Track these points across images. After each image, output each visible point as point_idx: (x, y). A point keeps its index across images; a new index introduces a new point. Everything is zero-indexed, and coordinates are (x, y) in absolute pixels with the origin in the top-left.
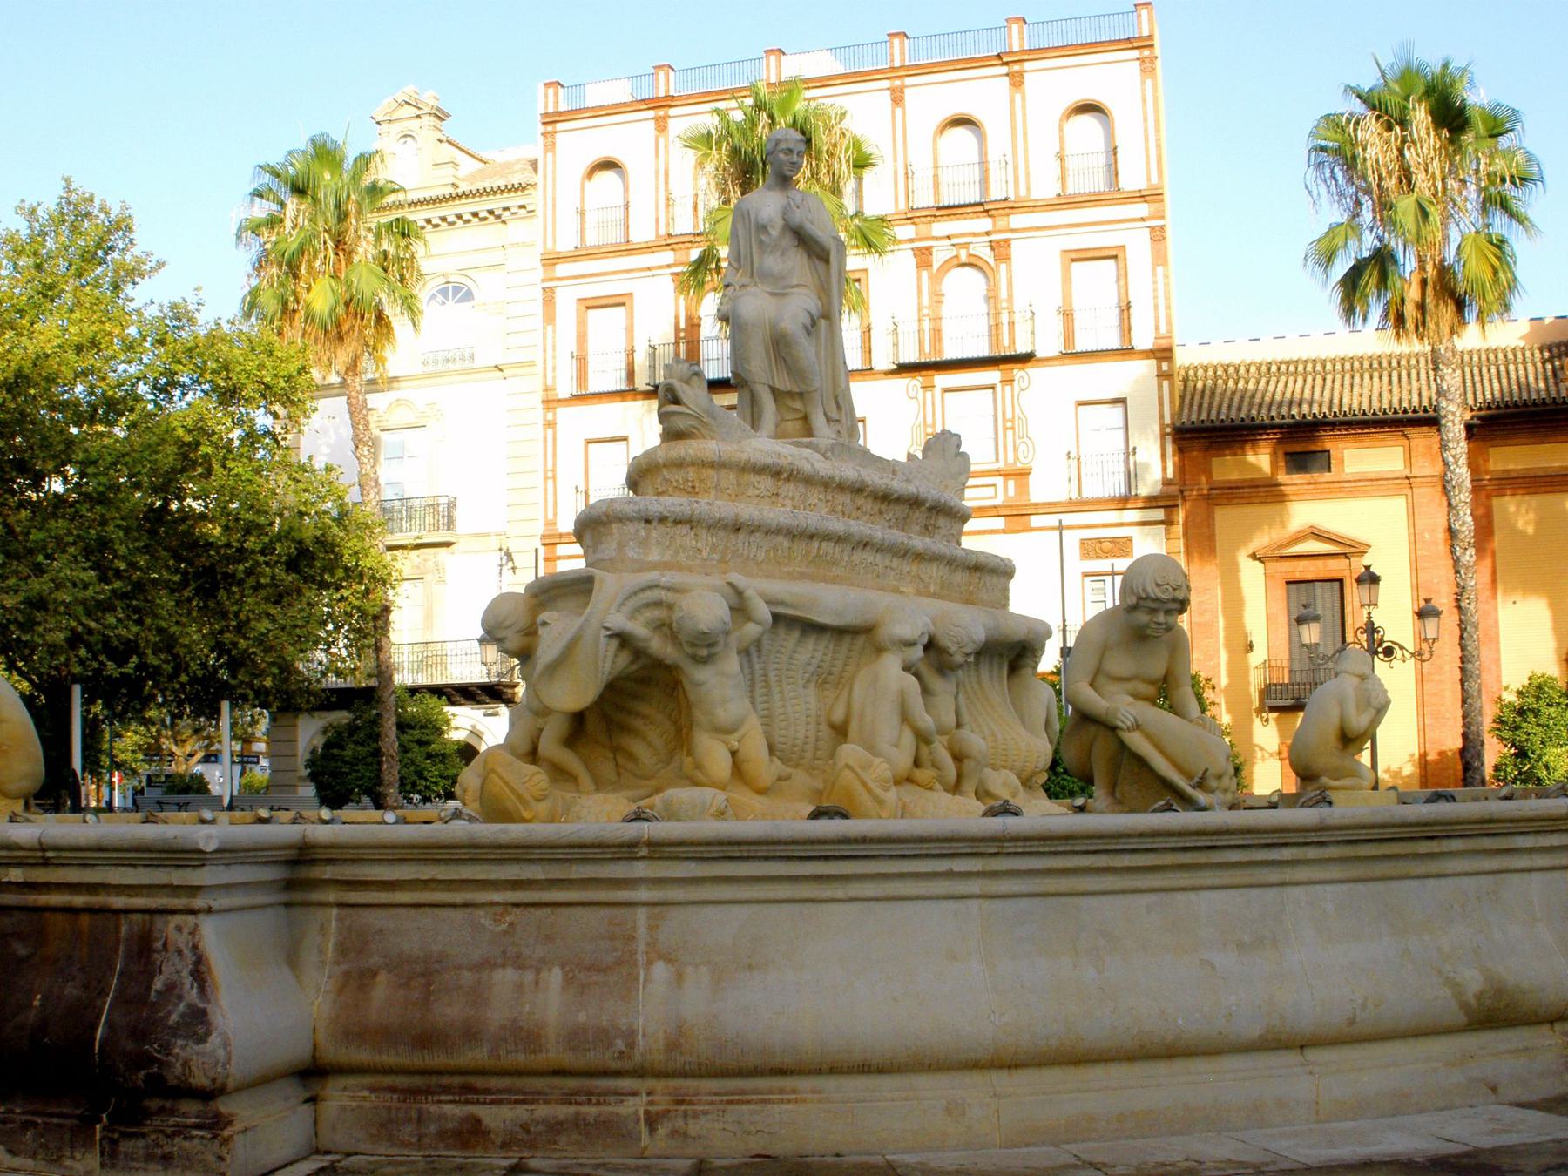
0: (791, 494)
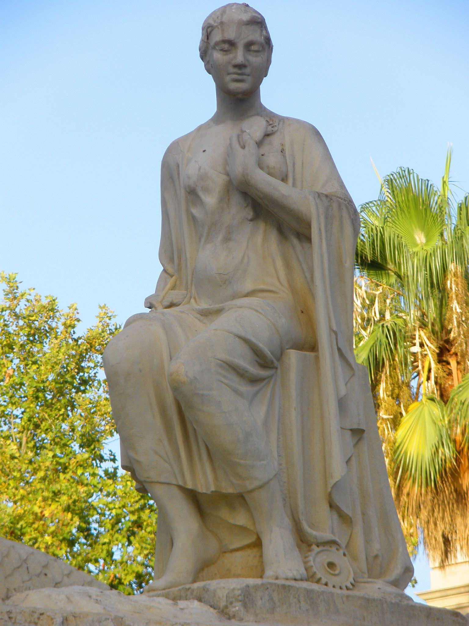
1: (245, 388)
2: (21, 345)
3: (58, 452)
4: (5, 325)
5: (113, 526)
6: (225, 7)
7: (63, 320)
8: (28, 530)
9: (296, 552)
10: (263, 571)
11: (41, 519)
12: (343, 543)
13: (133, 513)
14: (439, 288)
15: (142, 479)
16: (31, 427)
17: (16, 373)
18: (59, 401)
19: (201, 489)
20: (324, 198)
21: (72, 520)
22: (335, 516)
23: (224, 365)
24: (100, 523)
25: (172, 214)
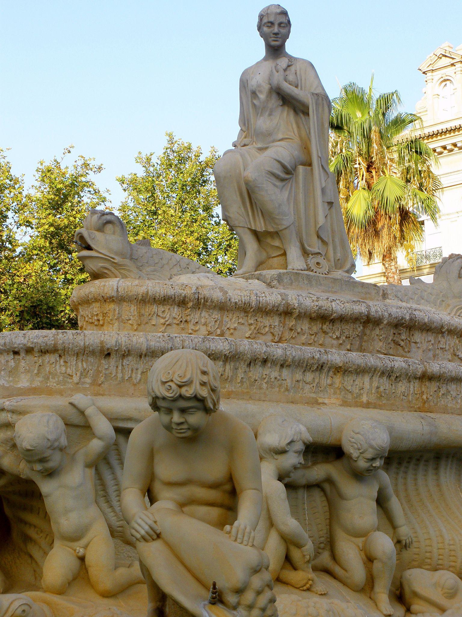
0: (203, 321)
1: (278, 183)
2: (175, 165)
3: (193, 213)
4: (168, 156)
5: (218, 247)
6: (269, 6)
7: (194, 154)
8: (180, 248)
9: (302, 258)
10: (287, 266)
11: (185, 244)
12: (323, 254)
13: (227, 241)
14: (367, 137)
15: (232, 225)
16: (180, 202)
17: (173, 178)
18: (193, 190)
19: (259, 229)
20: (315, 95)
21: (199, 244)
22: (320, 241)
23: (270, 174)
24: (212, 246)
25: (244, 103)
